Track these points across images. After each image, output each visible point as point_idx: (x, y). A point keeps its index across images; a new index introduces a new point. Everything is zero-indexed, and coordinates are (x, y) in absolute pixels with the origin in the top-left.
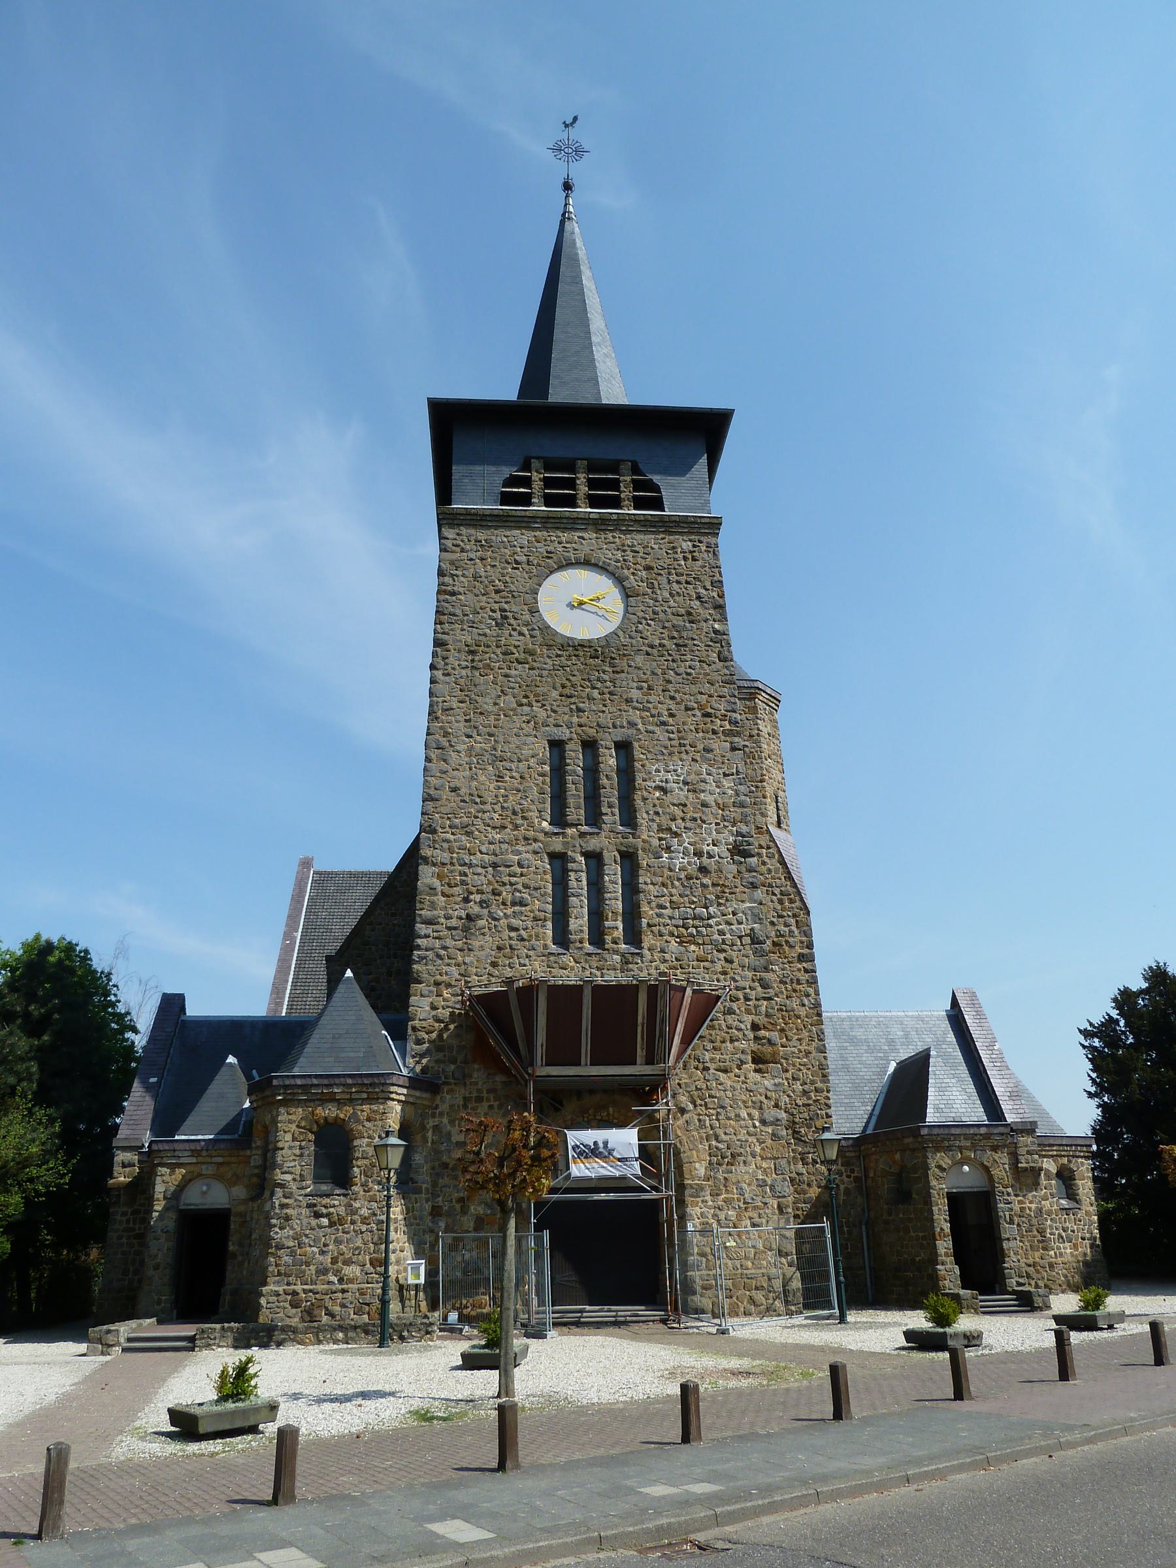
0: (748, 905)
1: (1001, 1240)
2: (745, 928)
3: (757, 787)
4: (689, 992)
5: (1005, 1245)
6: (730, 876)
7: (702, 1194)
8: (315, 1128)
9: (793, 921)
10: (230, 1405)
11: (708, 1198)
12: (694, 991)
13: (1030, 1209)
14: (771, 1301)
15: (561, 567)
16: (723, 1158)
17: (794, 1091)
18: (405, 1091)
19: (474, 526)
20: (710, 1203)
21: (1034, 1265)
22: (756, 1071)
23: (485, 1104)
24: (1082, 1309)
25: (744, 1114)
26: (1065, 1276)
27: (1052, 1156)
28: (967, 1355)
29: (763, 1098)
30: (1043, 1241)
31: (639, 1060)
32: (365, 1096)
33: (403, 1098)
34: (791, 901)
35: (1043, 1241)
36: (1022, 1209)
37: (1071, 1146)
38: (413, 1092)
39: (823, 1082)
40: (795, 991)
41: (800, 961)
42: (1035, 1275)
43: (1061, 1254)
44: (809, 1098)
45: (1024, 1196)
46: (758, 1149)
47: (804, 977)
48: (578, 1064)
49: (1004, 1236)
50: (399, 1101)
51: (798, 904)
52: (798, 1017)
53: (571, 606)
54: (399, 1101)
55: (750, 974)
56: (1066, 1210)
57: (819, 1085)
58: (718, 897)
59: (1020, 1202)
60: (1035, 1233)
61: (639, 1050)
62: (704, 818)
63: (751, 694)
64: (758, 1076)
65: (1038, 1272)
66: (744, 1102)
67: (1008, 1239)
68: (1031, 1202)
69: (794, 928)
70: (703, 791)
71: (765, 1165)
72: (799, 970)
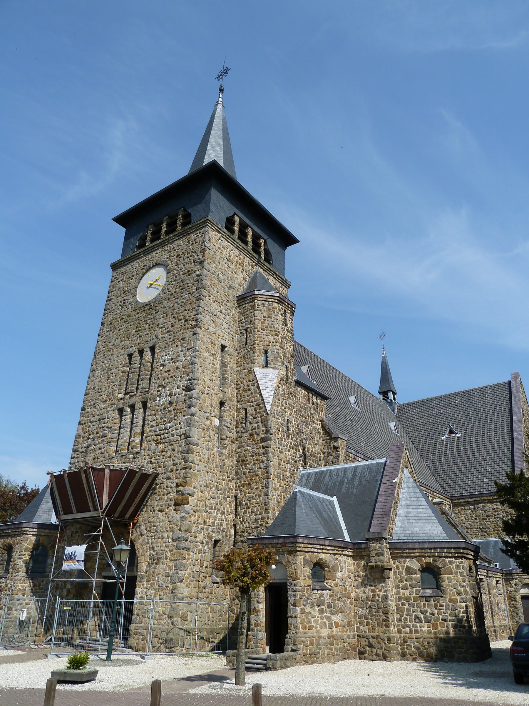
0: (186, 417)
1: (286, 618)
2: (182, 431)
3: (251, 348)
4: (107, 471)
5: (290, 621)
6: (181, 403)
7: (143, 580)
8: (5, 548)
9: (260, 419)
10: (72, 671)
11: (145, 583)
12: (111, 470)
13: (379, 596)
14: (159, 645)
15: (147, 271)
16: (154, 560)
17: (251, 520)
18: (36, 530)
19: (121, 267)
20: (145, 586)
21: (378, 637)
22: (175, 510)
23: (78, 534)
24: (69, 668)
25: (165, 535)
26: (418, 648)
27: (416, 557)
28: (57, 688)
29: (174, 526)
30: (386, 620)
31: (91, 510)
32: (17, 533)
33: (36, 533)
34: (260, 408)
35: (386, 620)
36: (374, 596)
37: (431, 549)
38: (41, 530)
39: (266, 513)
40: (257, 460)
41: (261, 442)
42: (377, 646)
43: (416, 631)
44: (258, 523)
45: (375, 586)
46: (169, 555)
47: (262, 451)
48: (72, 513)
49: (289, 614)
50: (33, 535)
51: (263, 409)
52: (257, 475)
53: (148, 288)
54: (33, 535)
55: (180, 456)
56: (427, 598)
57: (264, 515)
58: (175, 416)
59: (373, 591)
60: (381, 614)
61: (90, 504)
62: (176, 375)
63: (252, 298)
64: (175, 513)
65: (379, 643)
66: (166, 528)
67: (291, 617)
68: (380, 591)
69: (260, 424)
70: (178, 361)
71: (170, 564)
72: (260, 447)
